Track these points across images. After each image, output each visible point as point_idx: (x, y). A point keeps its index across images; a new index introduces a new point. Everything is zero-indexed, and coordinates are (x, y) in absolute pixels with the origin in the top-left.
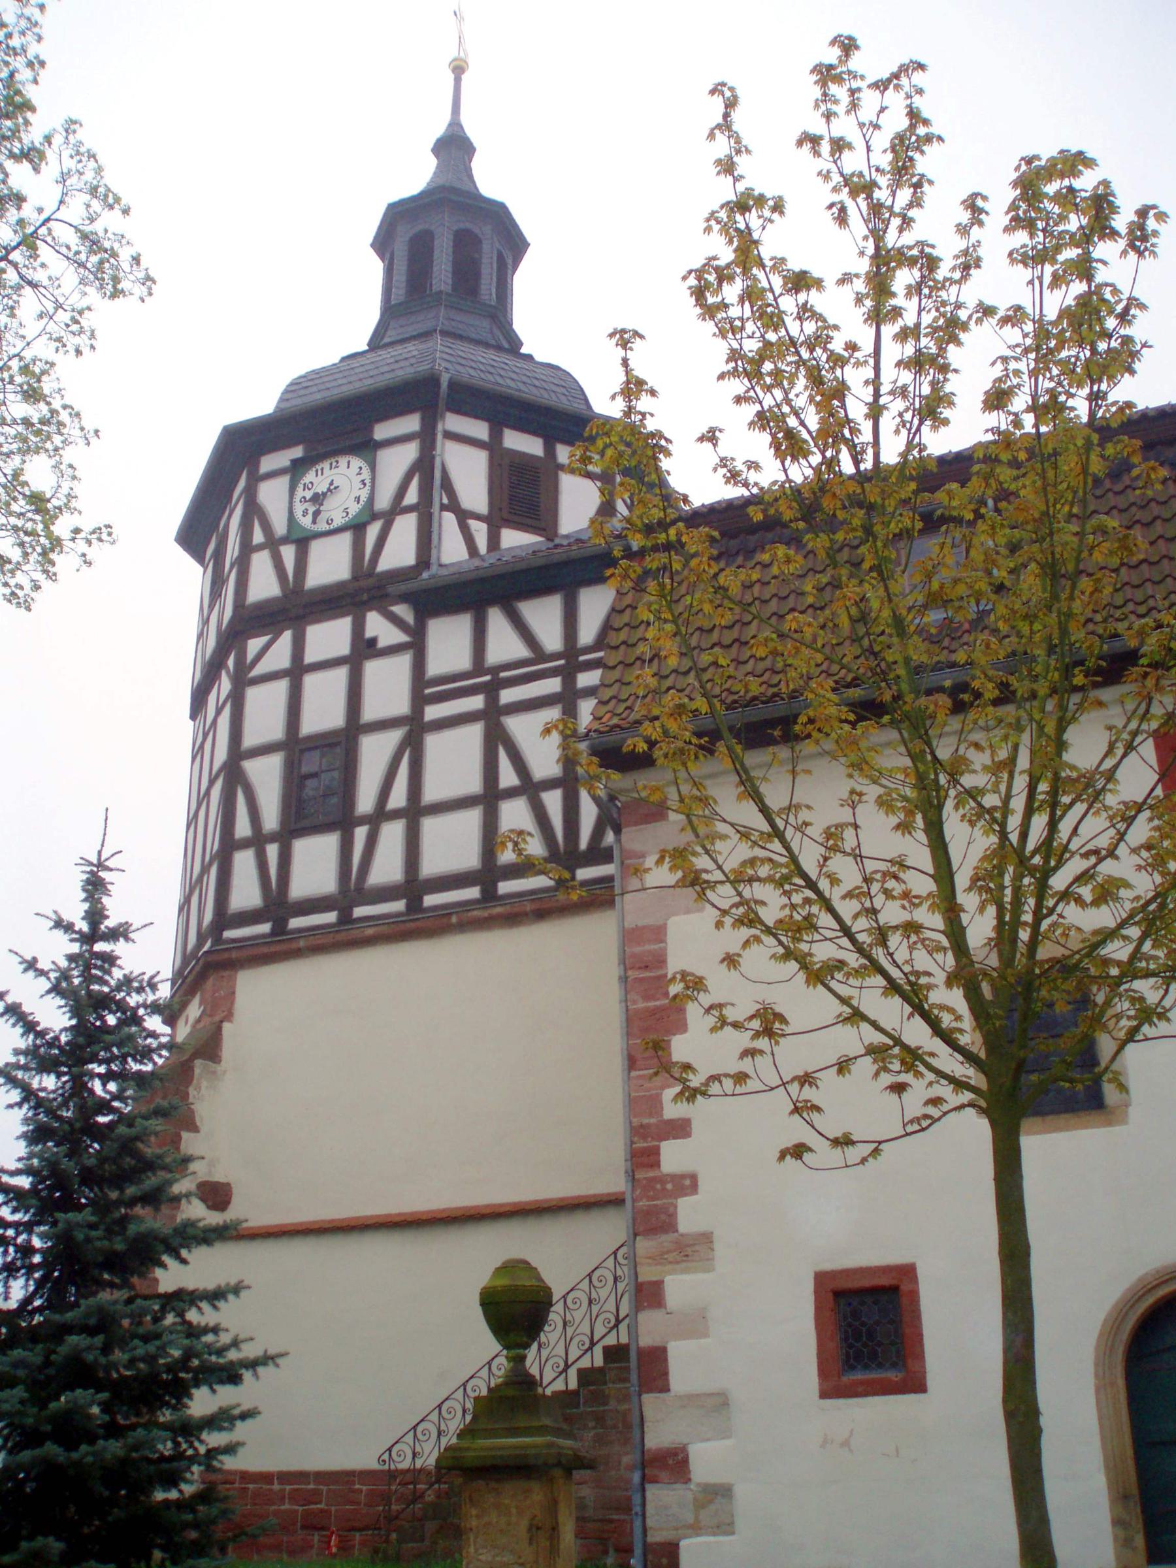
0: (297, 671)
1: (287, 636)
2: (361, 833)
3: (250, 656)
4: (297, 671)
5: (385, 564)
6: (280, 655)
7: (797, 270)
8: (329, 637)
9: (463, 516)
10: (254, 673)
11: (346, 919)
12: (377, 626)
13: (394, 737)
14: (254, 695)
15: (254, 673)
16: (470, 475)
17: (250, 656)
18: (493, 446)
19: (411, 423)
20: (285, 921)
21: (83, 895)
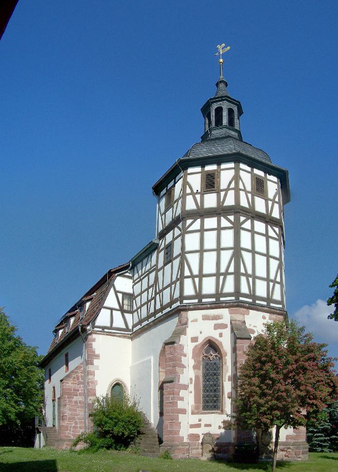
0: (202, 230)
1: (199, 221)
2: (222, 278)
3: (187, 225)
4: (202, 230)
5: (226, 204)
6: (197, 225)
7: (333, 295)
8: (211, 222)
9: (245, 190)
10: (188, 230)
11: (218, 299)
12: (224, 223)
13: (231, 252)
14: (188, 237)
15: (188, 230)
16: (246, 178)
17: (187, 225)
18: (251, 173)
19: (232, 165)
20: (199, 302)
21: (96, 362)
